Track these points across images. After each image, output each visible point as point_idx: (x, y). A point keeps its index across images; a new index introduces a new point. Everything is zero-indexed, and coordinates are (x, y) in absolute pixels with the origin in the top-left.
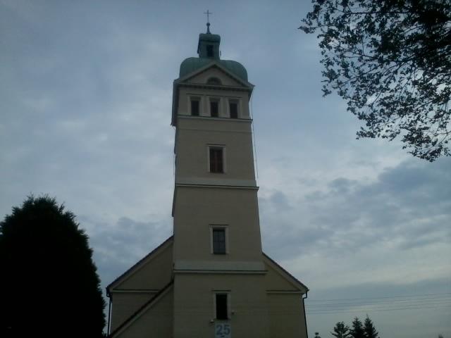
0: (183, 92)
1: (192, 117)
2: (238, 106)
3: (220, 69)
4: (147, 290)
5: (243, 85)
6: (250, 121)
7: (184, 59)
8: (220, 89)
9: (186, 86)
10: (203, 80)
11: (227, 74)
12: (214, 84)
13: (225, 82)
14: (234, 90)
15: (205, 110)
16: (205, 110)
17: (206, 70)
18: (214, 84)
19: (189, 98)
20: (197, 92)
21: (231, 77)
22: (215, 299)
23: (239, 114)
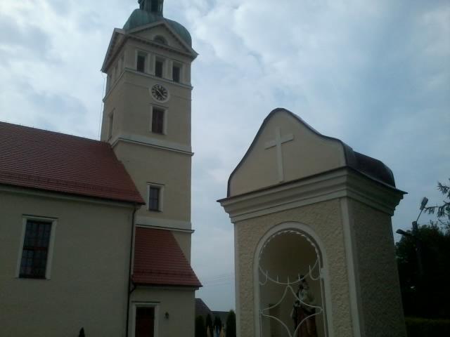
0: (129, 45)
1: (136, 72)
2: (146, 61)
3: (167, 29)
4: (61, 200)
5: (188, 51)
6: (190, 88)
7: (381, 160)
8: (162, 48)
9: (135, 39)
10: (151, 37)
11: (174, 36)
12: (159, 43)
13: (171, 43)
14: (179, 53)
15: (150, 69)
16: (150, 69)
17: (154, 27)
18: (159, 43)
19: (136, 52)
20: (162, 53)
21: (177, 40)
22: (149, 189)
23: (180, 76)
